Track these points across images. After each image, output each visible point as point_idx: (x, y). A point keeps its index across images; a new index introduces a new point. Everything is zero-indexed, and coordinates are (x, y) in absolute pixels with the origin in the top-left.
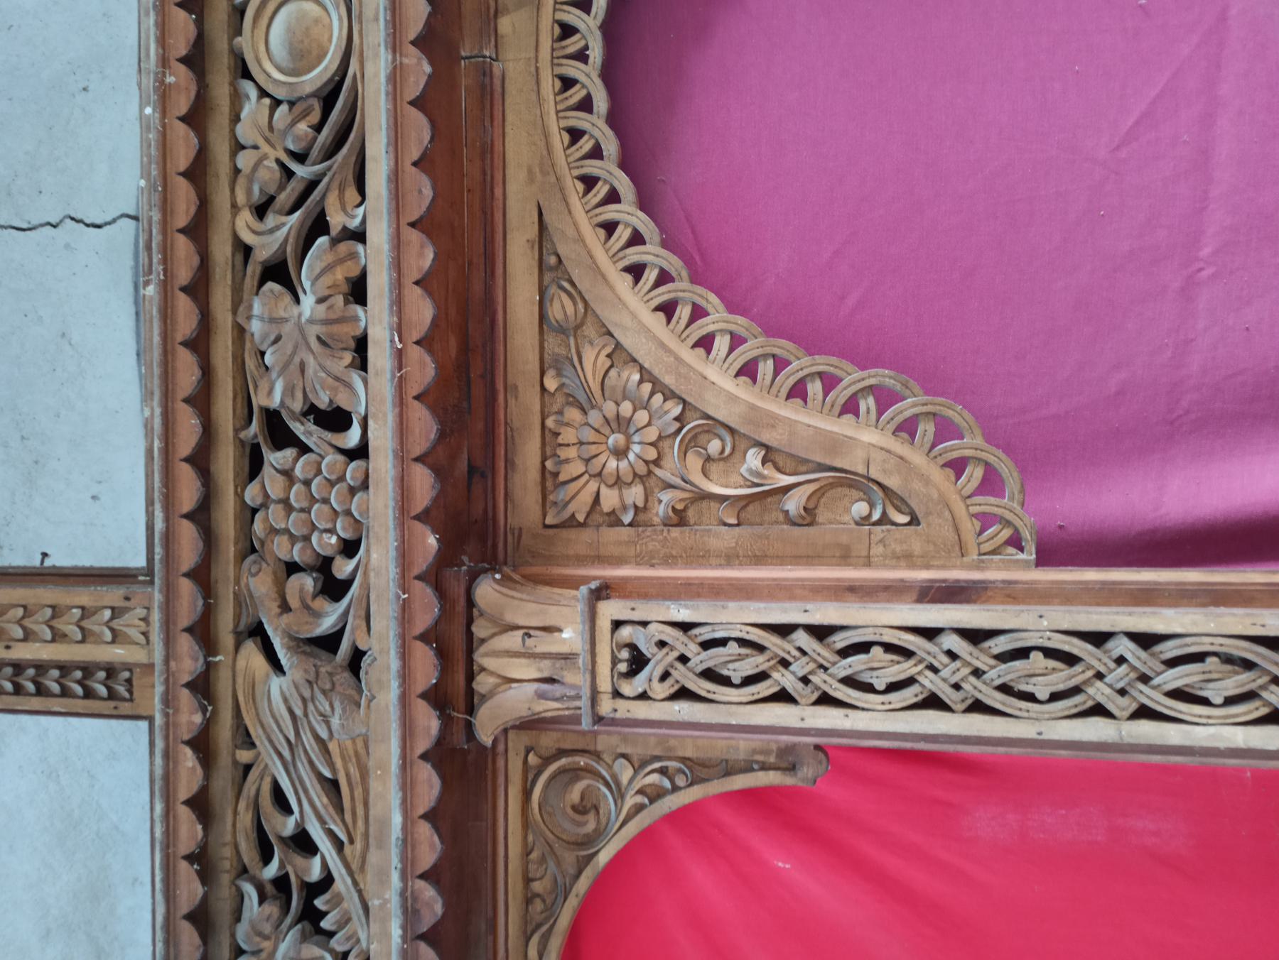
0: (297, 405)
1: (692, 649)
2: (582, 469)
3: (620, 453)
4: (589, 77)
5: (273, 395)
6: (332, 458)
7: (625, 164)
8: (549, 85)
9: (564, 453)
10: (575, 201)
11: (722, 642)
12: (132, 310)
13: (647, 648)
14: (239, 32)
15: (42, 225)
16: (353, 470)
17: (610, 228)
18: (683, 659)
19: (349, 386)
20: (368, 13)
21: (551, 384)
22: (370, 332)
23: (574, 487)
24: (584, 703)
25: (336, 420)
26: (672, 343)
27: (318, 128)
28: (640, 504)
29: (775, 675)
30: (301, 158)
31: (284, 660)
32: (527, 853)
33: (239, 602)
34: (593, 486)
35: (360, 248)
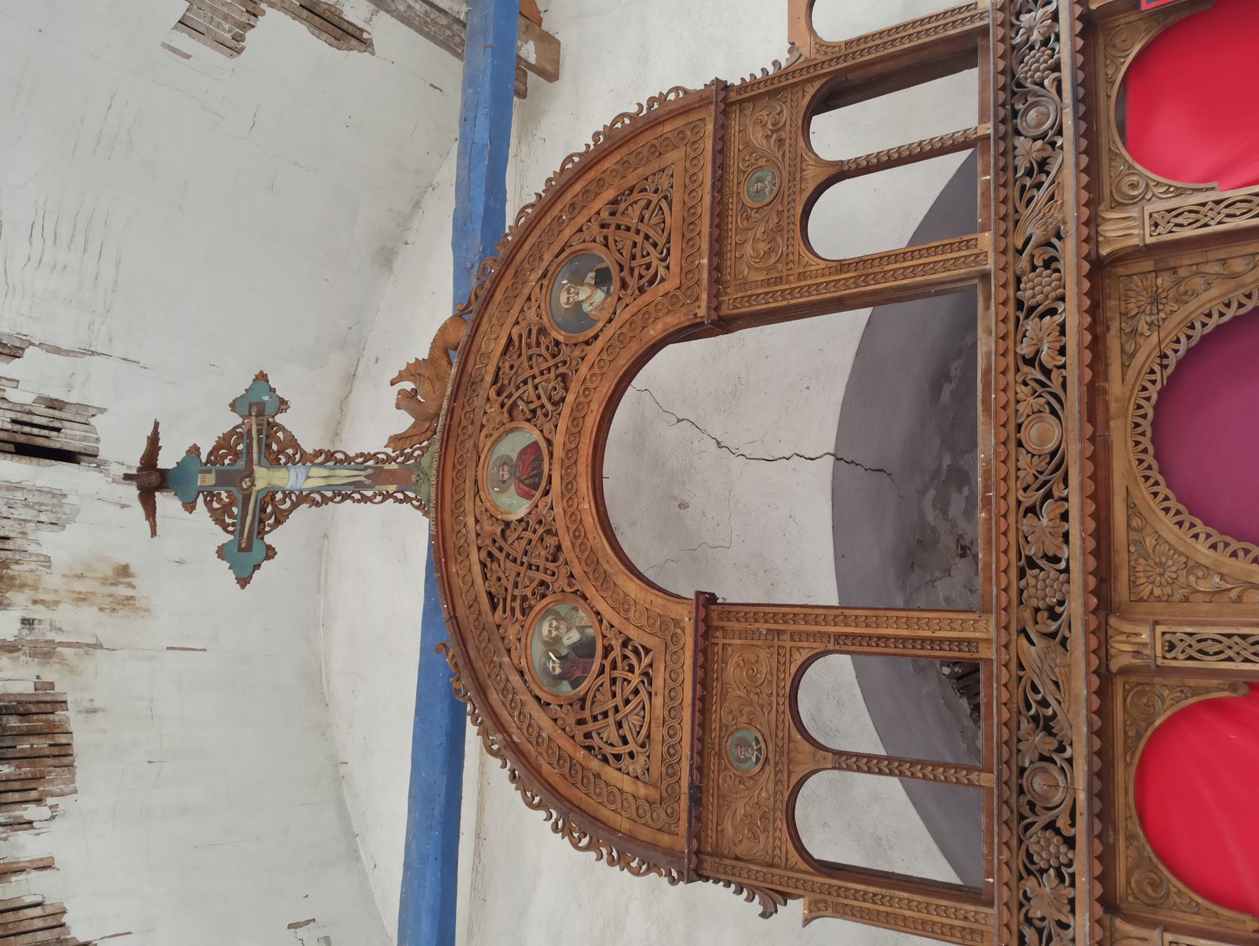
0: (1041, 555)
1: (1194, 643)
2: (1145, 581)
3: (1161, 575)
4: (1146, 442)
5: (1032, 551)
6: (1053, 574)
7: (1161, 472)
8: (1131, 444)
9: (1137, 575)
10: (1142, 485)
11: (1205, 640)
12: (831, 503)
13: (1176, 642)
14: (1019, 432)
15: (781, 458)
16: (1062, 577)
17: (1155, 494)
18: (1190, 646)
19: (1061, 548)
20: (1070, 428)
21: (1132, 549)
22: (1070, 531)
23: (1142, 587)
24: (1151, 661)
25: (1055, 560)
26: (1183, 536)
27: (1049, 464)
28: (1170, 593)
29: (1226, 651)
30: (1041, 473)
31: (1035, 640)
32: (1125, 722)
33: (1018, 621)
34: (1150, 586)
35: (1066, 503)
